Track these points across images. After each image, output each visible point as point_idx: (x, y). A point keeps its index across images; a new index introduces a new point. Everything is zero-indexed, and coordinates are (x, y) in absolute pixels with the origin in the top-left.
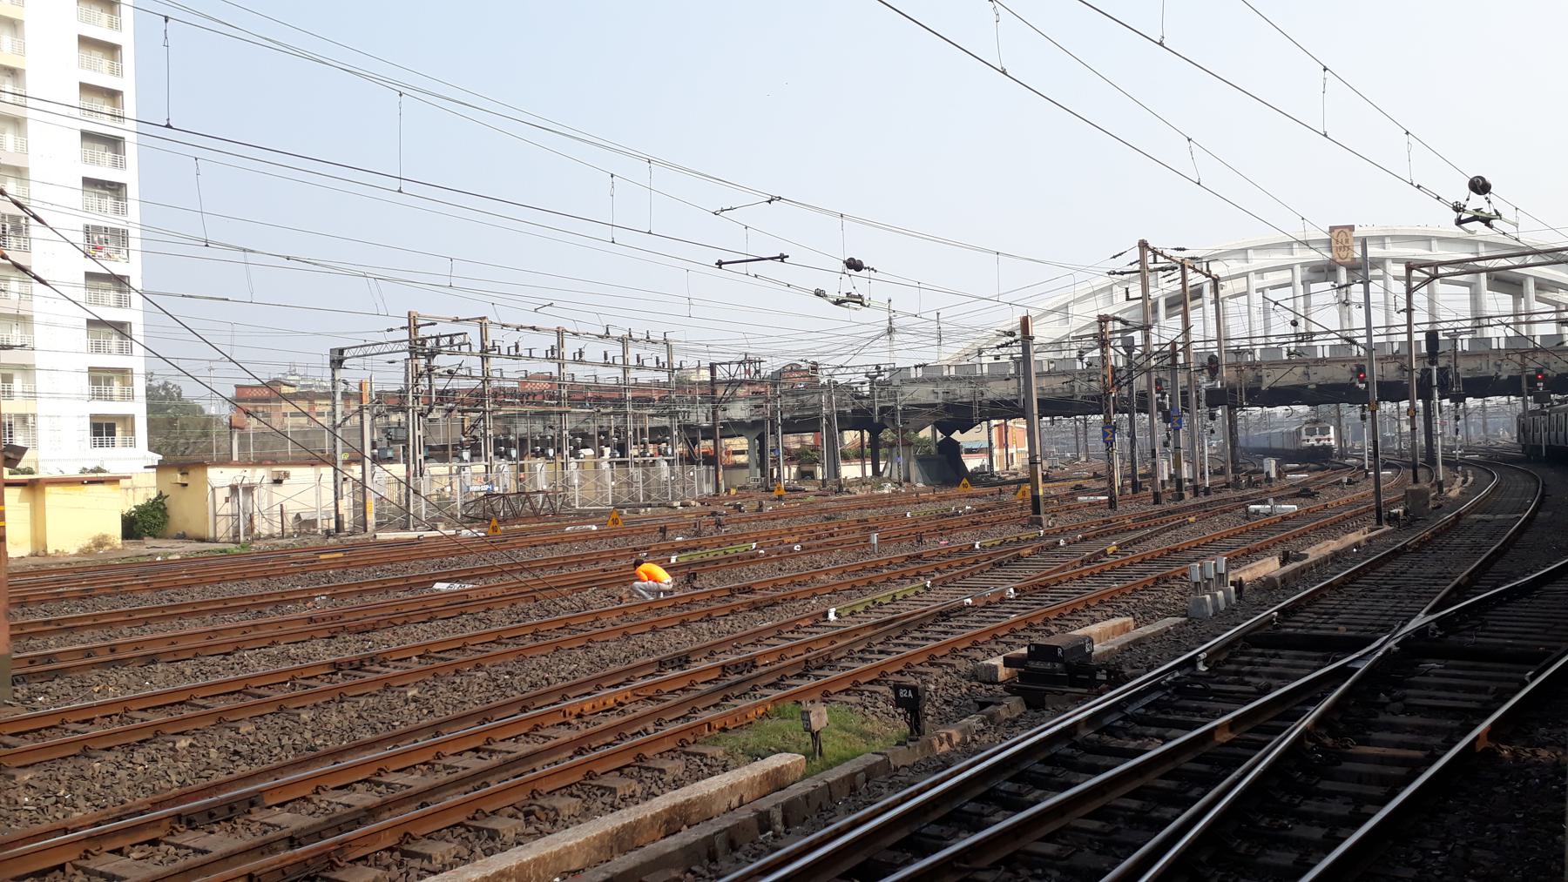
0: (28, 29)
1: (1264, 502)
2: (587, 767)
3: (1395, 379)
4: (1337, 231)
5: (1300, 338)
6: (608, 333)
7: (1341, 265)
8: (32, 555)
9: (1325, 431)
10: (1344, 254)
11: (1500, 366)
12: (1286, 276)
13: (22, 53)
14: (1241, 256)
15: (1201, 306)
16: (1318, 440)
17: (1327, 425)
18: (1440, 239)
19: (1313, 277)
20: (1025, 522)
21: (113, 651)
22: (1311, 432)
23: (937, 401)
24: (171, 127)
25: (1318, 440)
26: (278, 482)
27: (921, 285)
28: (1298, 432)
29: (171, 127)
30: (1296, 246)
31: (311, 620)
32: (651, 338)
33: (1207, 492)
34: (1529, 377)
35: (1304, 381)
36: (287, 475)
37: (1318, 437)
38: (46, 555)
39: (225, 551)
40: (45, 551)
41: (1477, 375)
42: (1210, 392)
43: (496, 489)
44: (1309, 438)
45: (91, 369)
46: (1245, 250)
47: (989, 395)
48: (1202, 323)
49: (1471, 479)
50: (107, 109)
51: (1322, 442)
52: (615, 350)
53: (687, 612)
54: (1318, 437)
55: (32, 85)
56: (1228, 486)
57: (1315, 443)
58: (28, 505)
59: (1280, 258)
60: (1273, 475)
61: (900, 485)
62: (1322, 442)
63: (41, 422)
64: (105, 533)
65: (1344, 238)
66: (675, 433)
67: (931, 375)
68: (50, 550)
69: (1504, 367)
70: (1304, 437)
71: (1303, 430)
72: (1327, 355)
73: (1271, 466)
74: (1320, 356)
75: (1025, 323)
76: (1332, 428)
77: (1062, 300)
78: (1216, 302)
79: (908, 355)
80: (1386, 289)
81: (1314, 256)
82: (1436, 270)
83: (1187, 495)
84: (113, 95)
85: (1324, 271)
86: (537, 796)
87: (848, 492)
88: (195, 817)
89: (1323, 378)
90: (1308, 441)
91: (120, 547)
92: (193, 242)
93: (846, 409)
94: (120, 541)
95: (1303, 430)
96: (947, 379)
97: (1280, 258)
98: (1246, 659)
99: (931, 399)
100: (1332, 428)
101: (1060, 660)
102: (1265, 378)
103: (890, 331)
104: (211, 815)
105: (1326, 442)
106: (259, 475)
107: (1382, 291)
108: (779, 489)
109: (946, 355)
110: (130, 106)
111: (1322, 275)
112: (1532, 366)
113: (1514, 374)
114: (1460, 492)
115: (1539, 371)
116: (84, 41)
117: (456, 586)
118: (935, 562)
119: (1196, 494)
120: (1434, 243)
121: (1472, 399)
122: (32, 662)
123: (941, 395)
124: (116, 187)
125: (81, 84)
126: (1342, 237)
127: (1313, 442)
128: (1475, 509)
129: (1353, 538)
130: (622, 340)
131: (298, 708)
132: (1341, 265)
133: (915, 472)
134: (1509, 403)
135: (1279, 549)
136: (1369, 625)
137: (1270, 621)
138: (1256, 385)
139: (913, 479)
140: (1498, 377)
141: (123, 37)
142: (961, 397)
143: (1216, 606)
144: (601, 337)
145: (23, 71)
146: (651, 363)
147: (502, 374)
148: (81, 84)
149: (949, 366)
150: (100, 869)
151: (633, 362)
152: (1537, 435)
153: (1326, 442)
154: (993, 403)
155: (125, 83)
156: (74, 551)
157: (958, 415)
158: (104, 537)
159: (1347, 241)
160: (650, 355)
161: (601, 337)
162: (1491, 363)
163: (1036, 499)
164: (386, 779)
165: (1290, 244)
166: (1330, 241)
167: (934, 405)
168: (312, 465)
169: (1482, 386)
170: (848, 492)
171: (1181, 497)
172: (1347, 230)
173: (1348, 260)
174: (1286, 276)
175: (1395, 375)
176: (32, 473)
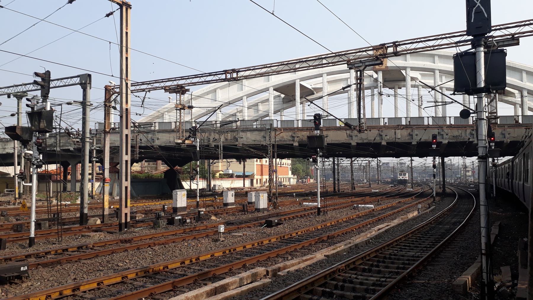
9: (405, 175)
16: (403, 177)
22: (401, 175)
24: (273, 15)
29: (273, 15)
35: (378, 140)
37: (403, 176)
41: (459, 140)
44: (400, 176)
47: (157, 143)
51: (404, 178)
53: (359, 224)
54: (403, 176)
57: (402, 178)
62: (404, 178)
70: (398, 176)
71: (398, 175)
72: (431, 123)
74: (426, 123)
76: (407, 174)
90: (399, 177)
93: (70, 148)
95: (398, 175)
100: (407, 174)
105: (405, 178)
120: (436, 58)
127: (401, 178)
164: (95, 248)
175: (407, 138)
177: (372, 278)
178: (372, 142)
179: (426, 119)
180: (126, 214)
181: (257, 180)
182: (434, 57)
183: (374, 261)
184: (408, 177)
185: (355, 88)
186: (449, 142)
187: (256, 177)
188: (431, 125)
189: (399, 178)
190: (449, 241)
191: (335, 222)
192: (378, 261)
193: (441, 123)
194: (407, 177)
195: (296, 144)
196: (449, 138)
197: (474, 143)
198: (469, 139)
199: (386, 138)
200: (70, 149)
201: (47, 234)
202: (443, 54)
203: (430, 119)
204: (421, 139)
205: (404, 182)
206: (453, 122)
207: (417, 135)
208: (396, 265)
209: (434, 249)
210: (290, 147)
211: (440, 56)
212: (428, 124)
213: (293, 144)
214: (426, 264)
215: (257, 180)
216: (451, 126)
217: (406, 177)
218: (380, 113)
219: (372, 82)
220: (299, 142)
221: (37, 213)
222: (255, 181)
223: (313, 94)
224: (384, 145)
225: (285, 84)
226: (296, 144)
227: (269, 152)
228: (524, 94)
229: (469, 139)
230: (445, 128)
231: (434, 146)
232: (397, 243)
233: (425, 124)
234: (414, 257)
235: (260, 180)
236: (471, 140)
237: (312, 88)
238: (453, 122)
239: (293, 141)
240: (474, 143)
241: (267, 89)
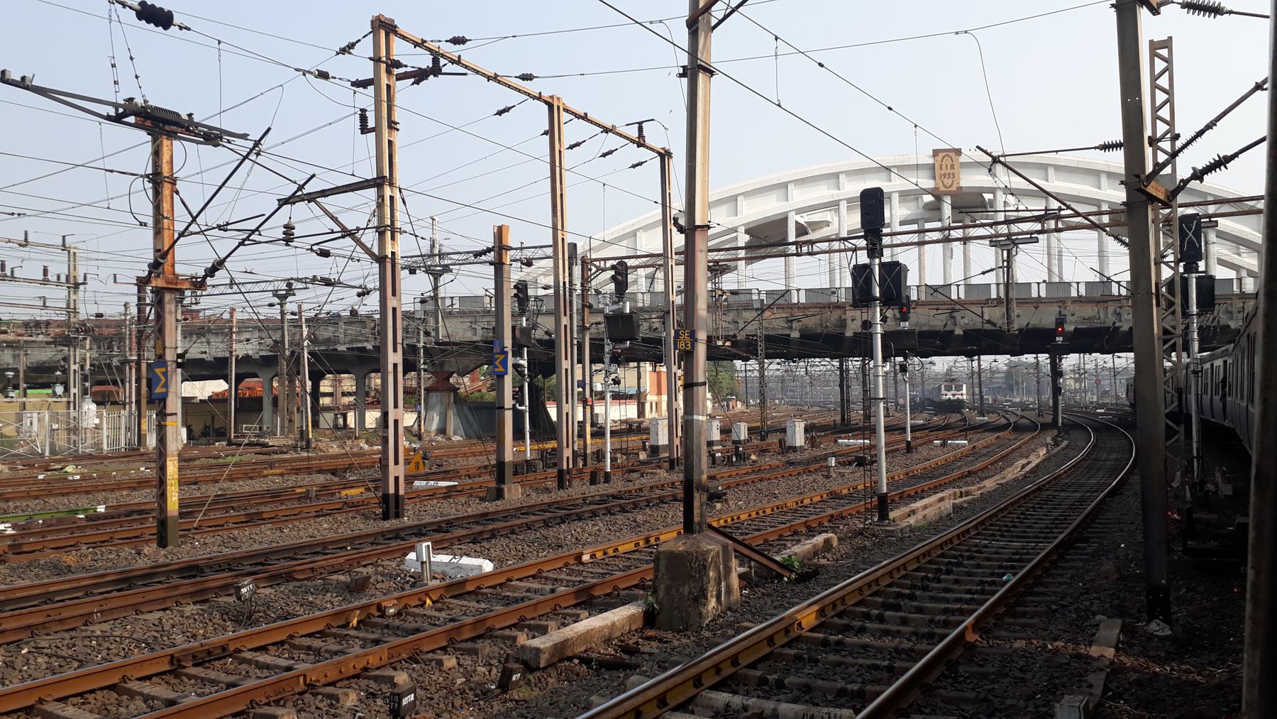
4: (941, 155)
5: (805, 249)
9: (959, 388)
10: (948, 181)
11: (1119, 314)
14: (833, 181)
16: (954, 395)
17: (960, 383)
22: (949, 389)
23: (475, 339)
28: (939, 388)
37: (954, 392)
41: (1094, 325)
44: (947, 392)
51: (956, 397)
54: (954, 392)
57: (952, 397)
62: (956, 397)
65: (949, 162)
70: (943, 392)
71: (943, 388)
72: (1043, 295)
74: (1034, 295)
75: (500, 233)
76: (964, 386)
77: (629, 227)
86: (255, 705)
93: (366, 344)
95: (943, 388)
99: (469, 336)
100: (964, 386)
102: (849, 322)
105: (960, 397)
114: (955, 507)
120: (1051, 171)
123: (480, 332)
126: (948, 161)
127: (949, 396)
132: (946, 194)
133: (453, 422)
136: (1013, 554)
138: (838, 330)
139: (450, 429)
147: (44, 303)
159: (952, 167)
163: (501, 465)
166: (933, 167)
172: (952, 155)
173: (954, 188)
177: (1075, 494)
178: (941, 329)
179: (1034, 287)
180: (397, 479)
181: (651, 404)
182: (1047, 171)
183: (928, 571)
184: (967, 394)
185: (826, 187)
186: (1076, 329)
187: (649, 398)
188: (1043, 298)
189: (944, 397)
190: (1039, 572)
191: (822, 497)
192: (913, 587)
193: (1061, 295)
194: (964, 394)
195: (795, 335)
196: (1076, 322)
197: (1121, 329)
198: (1114, 323)
199: (962, 322)
200: (367, 348)
201: (215, 526)
202: (1062, 164)
203: (1043, 286)
204: (1028, 324)
205: (956, 406)
206: (1083, 292)
207: (1018, 316)
208: (927, 617)
209: (1081, 518)
210: (785, 340)
211: (1058, 168)
212: (1039, 296)
213: (789, 335)
214: (1054, 557)
215: (651, 404)
216: (1079, 300)
217: (962, 395)
218: (947, 274)
219: (920, 210)
220: (800, 331)
221: (182, 482)
222: (647, 406)
223: (806, 233)
224: (959, 335)
225: (768, 221)
226: (795, 335)
227: (759, 352)
228: (1210, 239)
229: (1114, 323)
230: (1069, 303)
231: (1059, 339)
232: (940, 552)
233: (1033, 296)
234: (974, 594)
235: (656, 403)
236: (1117, 325)
237: (806, 222)
238: (1083, 292)
239: (791, 328)
240: (1121, 329)
241: (735, 230)
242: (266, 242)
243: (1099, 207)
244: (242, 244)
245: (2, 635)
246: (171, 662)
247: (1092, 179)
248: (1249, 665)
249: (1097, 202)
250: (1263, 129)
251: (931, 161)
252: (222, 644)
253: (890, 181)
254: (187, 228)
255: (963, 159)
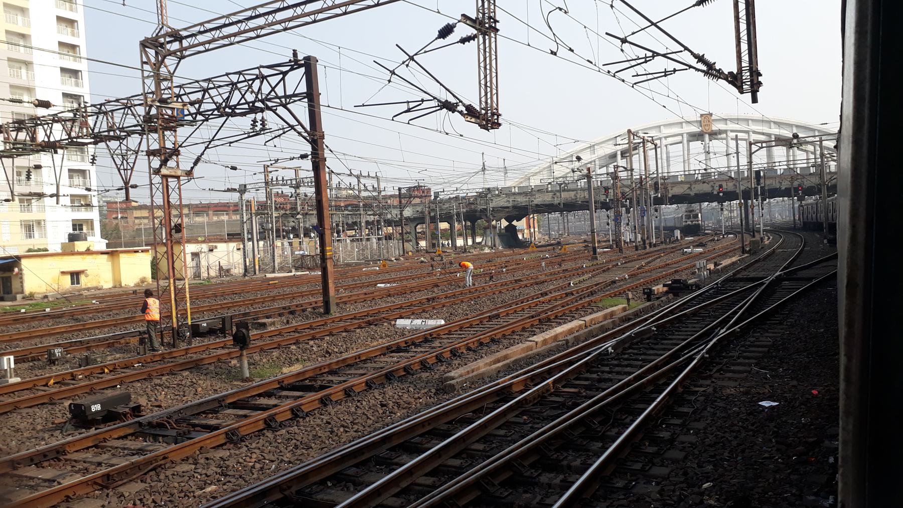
0: (31, 13)
1: (688, 248)
2: (531, 323)
3: (732, 190)
6: (351, 173)
7: (706, 133)
8: (113, 287)
11: (781, 183)
12: (679, 138)
13: (29, 26)
15: (638, 153)
18: (752, 120)
19: (691, 139)
20: (590, 258)
21: (316, 303)
23: (509, 205)
25: (692, 222)
26: (211, 250)
27: (509, 149)
30: (684, 124)
31: (366, 294)
32: (363, 175)
33: (655, 245)
34: (794, 188)
36: (216, 247)
37: (692, 219)
38: (121, 287)
39: (202, 283)
40: (120, 285)
42: (656, 198)
43: (306, 253)
45: (72, 196)
46: (659, 127)
48: (637, 162)
49: (771, 237)
50: (22, 43)
52: (354, 181)
54: (692, 219)
55: (34, 42)
56: (662, 243)
57: (690, 223)
58: (110, 263)
59: (676, 130)
60: (679, 238)
61: (492, 248)
63: (48, 225)
64: (145, 276)
66: (383, 224)
67: (506, 192)
68: (123, 285)
69: (783, 183)
73: (678, 233)
78: (644, 152)
79: (496, 181)
80: (727, 146)
81: (695, 129)
82: (762, 145)
83: (648, 247)
84: (73, 47)
85: (697, 137)
87: (470, 252)
88: (47, 453)
89: (698, 190)
91: (151, 283)
92: (389, 162)
94: (151, 280)
96: (514, 194)
97: (676, 130)
98: (607, 369)
99: (506, 204)
101: (682, 283)
103: (484, 169)
104: (45, 456)
105: (697, 222)
106: (205, 247)
107: (725, 146)
108: (439, 251)
109: (511, 182)
110: (83, 52)
111: (695, 138)
112: (796, 184)
113: (787, 186)
115: (799, 185)
116: (60, 19)
117: (389, 285)
118: (453, 299)
119: (650, 247)
120: (750, 122)
121: (304, 71)
122: (297, 306)
124: (78, 97)
125: (6, 30)
128: (778, 247)
129: (734, 259)
130: (358, 177)
131: (103, 389)
132: (706, 133)
134: (783, 200)
135: (713, 261)
137: (731, 276)
139: (497, 245)
140: (780, 188)
141: (78, 15)
142: (521, 203)
143: (704, 277)
144: (349, 175)
145: (30, 36)
146: (370, 188)
148: (6, 30)
149: (515, 187)
150: (24, 474)
151: (362, 187)
152: (810, 216)
153: (697, 222)
154: (537, 205)
155: (80, 41)
156: (132, 285)
157: (520, 212)
158: (144, 278)
160: (369, 183)
161: (349, 175)
162: (777, 181)
165: (681, 123)
166: (701, 121)
167: (508, 207)
168: (225, 242)
169: (774, 193)
170: (470, 252)
171: (645, 248)
172: (709, 116)
173: (709, 131)
174: (679, 138)
176: (48, 251)
242: (222, 145)
243: (771, 137)
244: (207, 148)
245: (1, 418)
246: (539, 321)
247: (767, 125)
248: (844, 429)
249: (769, 135)
250: (745, 13)
251: (699, 119)
252: (43, 451)
253: (682, 128)
254: (44, 130)
255: (714, 117)
